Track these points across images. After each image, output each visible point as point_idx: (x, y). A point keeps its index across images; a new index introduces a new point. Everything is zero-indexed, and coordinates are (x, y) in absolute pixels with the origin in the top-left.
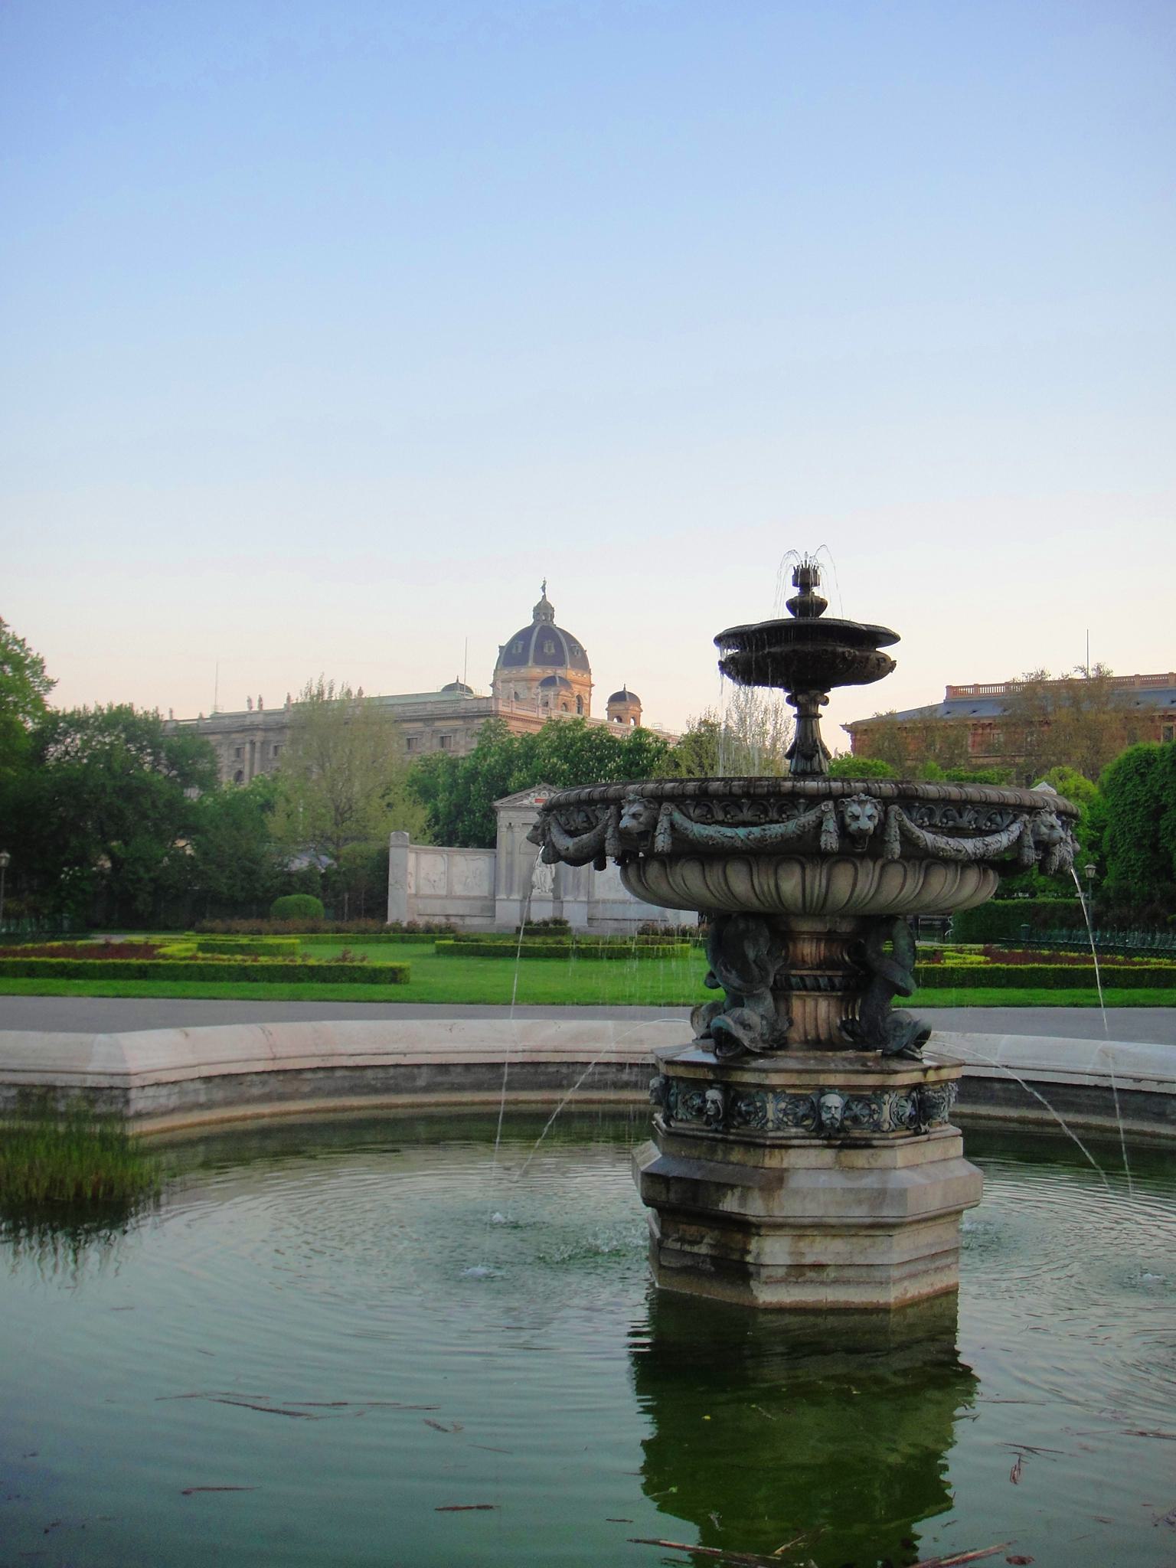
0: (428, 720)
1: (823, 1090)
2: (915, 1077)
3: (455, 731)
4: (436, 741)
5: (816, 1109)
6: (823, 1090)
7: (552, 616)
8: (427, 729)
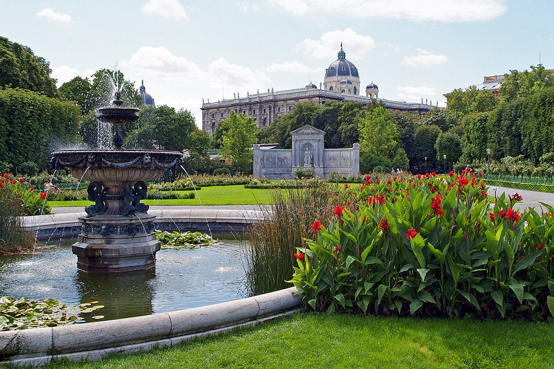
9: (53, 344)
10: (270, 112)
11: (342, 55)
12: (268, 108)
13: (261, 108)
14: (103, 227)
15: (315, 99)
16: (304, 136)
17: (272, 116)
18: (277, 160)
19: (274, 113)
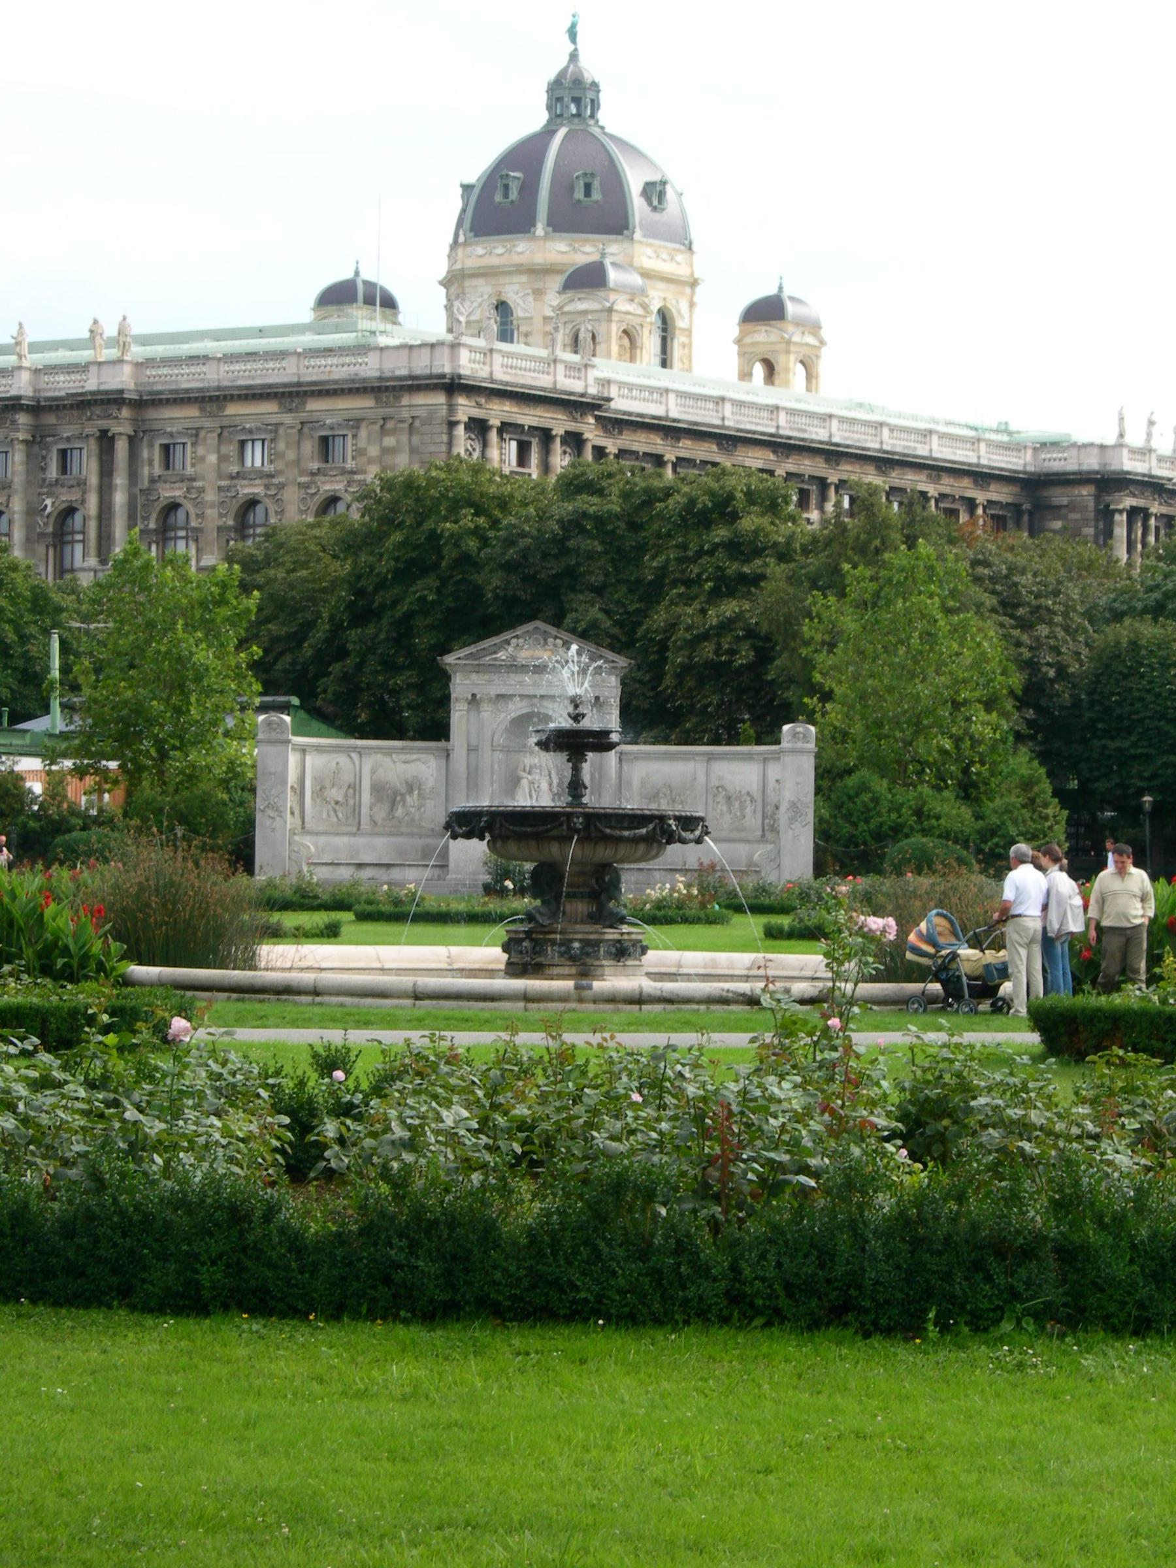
0: (291, 395)
1: (571, 941)
2: (617, 937)
3: (356, 423)
4: (309, 447)
5: (570, 948)
6: (571, 941)
7: (595, 104)
8: (288, 419)
9: (1044, 929)
10: (106, 472)
11: (572, 96)
12: (93, 445)
13: (37, 441)
14: (576, 945)
15: (421, 399)
16: (514, 678)
17: (120, 498)
18: (366, 797)
19: (133, 475)
